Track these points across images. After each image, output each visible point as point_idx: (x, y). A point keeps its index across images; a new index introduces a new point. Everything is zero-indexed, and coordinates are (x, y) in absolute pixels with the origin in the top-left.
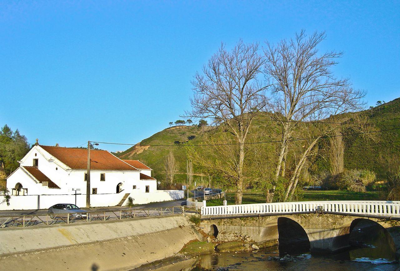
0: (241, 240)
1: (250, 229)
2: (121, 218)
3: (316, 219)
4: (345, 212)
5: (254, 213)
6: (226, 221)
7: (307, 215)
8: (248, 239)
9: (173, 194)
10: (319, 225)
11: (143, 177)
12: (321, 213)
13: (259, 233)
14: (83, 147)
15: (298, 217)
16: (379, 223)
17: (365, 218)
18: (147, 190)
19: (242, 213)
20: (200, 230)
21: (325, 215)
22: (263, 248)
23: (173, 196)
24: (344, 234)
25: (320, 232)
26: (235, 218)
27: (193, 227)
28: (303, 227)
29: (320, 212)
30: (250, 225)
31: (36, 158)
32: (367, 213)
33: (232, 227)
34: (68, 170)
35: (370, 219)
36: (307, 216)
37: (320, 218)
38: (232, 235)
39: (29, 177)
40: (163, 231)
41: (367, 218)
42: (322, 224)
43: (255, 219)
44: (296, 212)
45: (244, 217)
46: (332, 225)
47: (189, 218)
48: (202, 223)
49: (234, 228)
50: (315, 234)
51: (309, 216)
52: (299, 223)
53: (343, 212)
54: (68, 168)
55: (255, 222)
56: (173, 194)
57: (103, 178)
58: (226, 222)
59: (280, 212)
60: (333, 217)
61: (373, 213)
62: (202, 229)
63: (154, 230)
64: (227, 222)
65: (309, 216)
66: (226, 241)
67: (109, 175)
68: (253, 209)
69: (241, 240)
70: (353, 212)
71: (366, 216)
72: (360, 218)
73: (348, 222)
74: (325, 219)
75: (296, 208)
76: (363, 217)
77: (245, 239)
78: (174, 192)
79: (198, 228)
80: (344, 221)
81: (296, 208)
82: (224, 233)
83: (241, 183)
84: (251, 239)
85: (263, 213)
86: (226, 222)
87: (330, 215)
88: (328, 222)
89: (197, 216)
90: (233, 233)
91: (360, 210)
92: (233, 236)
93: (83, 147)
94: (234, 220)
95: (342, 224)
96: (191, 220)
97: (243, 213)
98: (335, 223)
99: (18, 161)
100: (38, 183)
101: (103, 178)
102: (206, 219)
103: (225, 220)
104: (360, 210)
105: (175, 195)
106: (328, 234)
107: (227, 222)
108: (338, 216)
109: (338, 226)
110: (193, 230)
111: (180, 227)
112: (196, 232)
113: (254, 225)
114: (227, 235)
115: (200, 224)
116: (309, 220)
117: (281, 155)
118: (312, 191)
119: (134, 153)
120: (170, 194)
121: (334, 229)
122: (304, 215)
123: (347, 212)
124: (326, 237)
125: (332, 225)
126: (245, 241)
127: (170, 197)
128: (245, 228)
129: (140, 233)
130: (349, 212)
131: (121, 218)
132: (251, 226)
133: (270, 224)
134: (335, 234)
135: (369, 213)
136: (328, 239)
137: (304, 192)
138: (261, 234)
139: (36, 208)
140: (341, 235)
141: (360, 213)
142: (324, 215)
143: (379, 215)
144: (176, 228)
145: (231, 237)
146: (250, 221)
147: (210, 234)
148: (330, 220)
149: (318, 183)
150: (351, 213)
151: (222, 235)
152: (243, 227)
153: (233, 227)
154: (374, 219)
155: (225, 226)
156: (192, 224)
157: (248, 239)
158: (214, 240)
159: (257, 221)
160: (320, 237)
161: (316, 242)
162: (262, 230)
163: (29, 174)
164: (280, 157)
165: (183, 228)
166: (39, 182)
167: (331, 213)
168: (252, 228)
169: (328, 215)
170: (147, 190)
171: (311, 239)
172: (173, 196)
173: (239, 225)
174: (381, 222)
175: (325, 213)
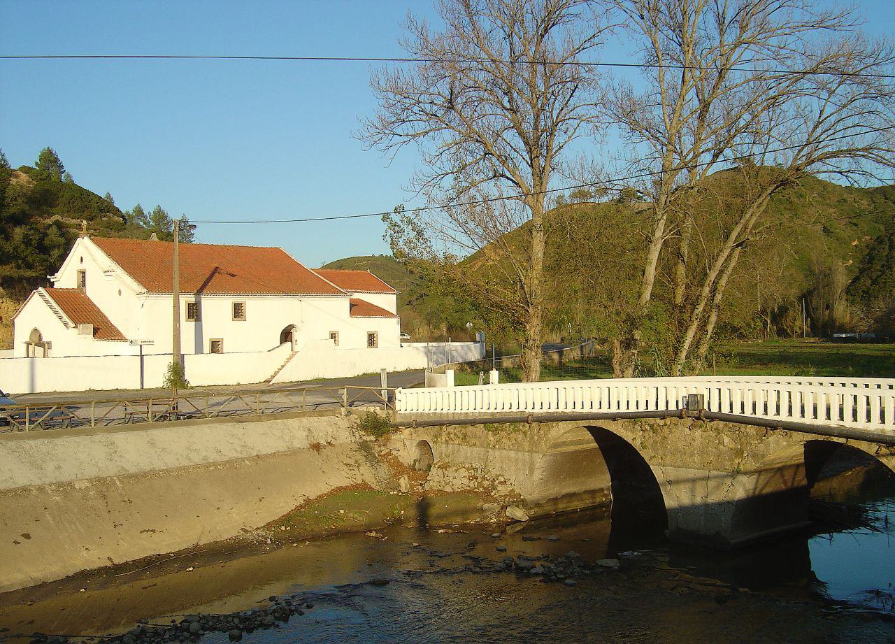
0: (484, 488)
1: (509, 459)
2: (93, 424)
3: (683, 433)
4: (771, 416)
5: (520, 410)
6: (452, 431)
7: (658, 420)
8: (500, 488)
9: (434, 353)
10: (692, 455)
11: (357, 309)
12: (698, 418)
13: (532, 470)
14: (384, 255)
15: (634, 428)
16: (884, 460)
17: (835, 439)
18: (372, 340)
19: (488, 411)
20: (389, 454)
21: (712, 424)
22: (547, 516)
23: (435, 357)
24: (783, 487)
25: (693, 481)
26: (473, 423)
27: (364, 447)
28: (646, 458)
29: (694, 412)
30: (509, 446)
31: (81, 267)
32: (841, 423)
33: (465, 450)
34: (141, 294)
35: (854, 443)
36: (659, 426)
37: (698, 433)
38: (463, 472)
39: (54, 316)
40: (232, 464)
41: (842, 440)
42: (703, 452)
43: (521, 428)
44: (639, 410)
45: (496, 423)
46: (731, 460)
47: (358, 421)
48: (395, 437)
49: (469, 454)
50: (681, 486)
51: (665, 424)
52: (637, 445)
53: (765, 417)
54: (140, 289)
55: (520, 436)
56: (434, 353)
57: (238, 311)
58: (452, 436)
59: (587, 410)
60: (734, 433)
61: (861, 424)
62: (394, 452)
63: (197, 459)
64: (455, 434)
65: (665, 424)
66: (448, 489)
67: (255, 305)
68: (628, 394)
69: (484, 488)
70: (796, 418)
71: (836, 432)
72: (820, 438)
73: (790, 450)
74: (711, 438)
75: (657, 398)
76: (830, 435)
77: (494, 488)
78: (441, 349)
79: (382, 448)
80: (767, 445)
81: (657, 398)
82: (444, 467)
83: (535, 321)
84: (509, 489)
85: (541, 411)
86: (452, 436)
87: (726, 425)
88: (722, 447)
89: (381, 413)
90: (468, 469)
91: (822, 412)
92: (464, 477)
93: (384, 255)
94: (470, 428)
95: (763, 456)
96: (364, 427)
97: (492, 410)
98: (739, 453)
99: (48, 277)
100: (70, 329)
101: (238, 311)
102: (409, 425)
103: (451, 429)
104: (822, 412)
105: (441, 356)
106: (717, 487)
107: (455, 434)
108: (751, 430)
109: (751, 465)
110: (360, 456)
111: (317, 447)
112: (371, 462)
113: (518, 447)
114: (450, 472)
115: (388, 440)
116: (665, 438)
117: (654, 239)
118: (850, 345)
119: (480, 263)
120: (428, 353)
121: (738, 472)
122: (651, 421)
123: (777, 418)
124: (712, 499)
125: (731, 460)
126: (493, 494)
127: (425, 359)
128: (497, 453)
129: (132, 470)
130: (784, 417)
131: (93, 424)
132: (511, 450)
133: (564, 444)
134: (741, 489)
135: (848, 423)
136: (720, 504)
137: (827, 348)
138: (537, 475)
139: (139, 387)
140: (767, 490)
141: (821, 421)
142: (709, 425)
143: (883, 430)
144: (295, 452)
145: (458, 481)
146: (509, 434)
147: (417, 467)
148: (726, 440)
149: (863, 326)
150: (790, 419)
151: (440, 471)
152: (490, 450)
153: (469, 449)
154: (863, 446)
155: (450, 446)
156: (364, 438)
157: (500, 488)
158: (421, 485)
159: (525, 433)
160: (693, 495)
161: (683, 510)
162: (540, 461)
163: (55, 305)
164: (652, 246)
165: (326, 451)
166: (72, 325)
167: (729, 419)
168: (512, 454)
169: (721, 424)
170: (372, 340)
171: (669, 502)
172: (435, 357)
173: (482, 446)
174: (889, 458)
175: (712, 417)
